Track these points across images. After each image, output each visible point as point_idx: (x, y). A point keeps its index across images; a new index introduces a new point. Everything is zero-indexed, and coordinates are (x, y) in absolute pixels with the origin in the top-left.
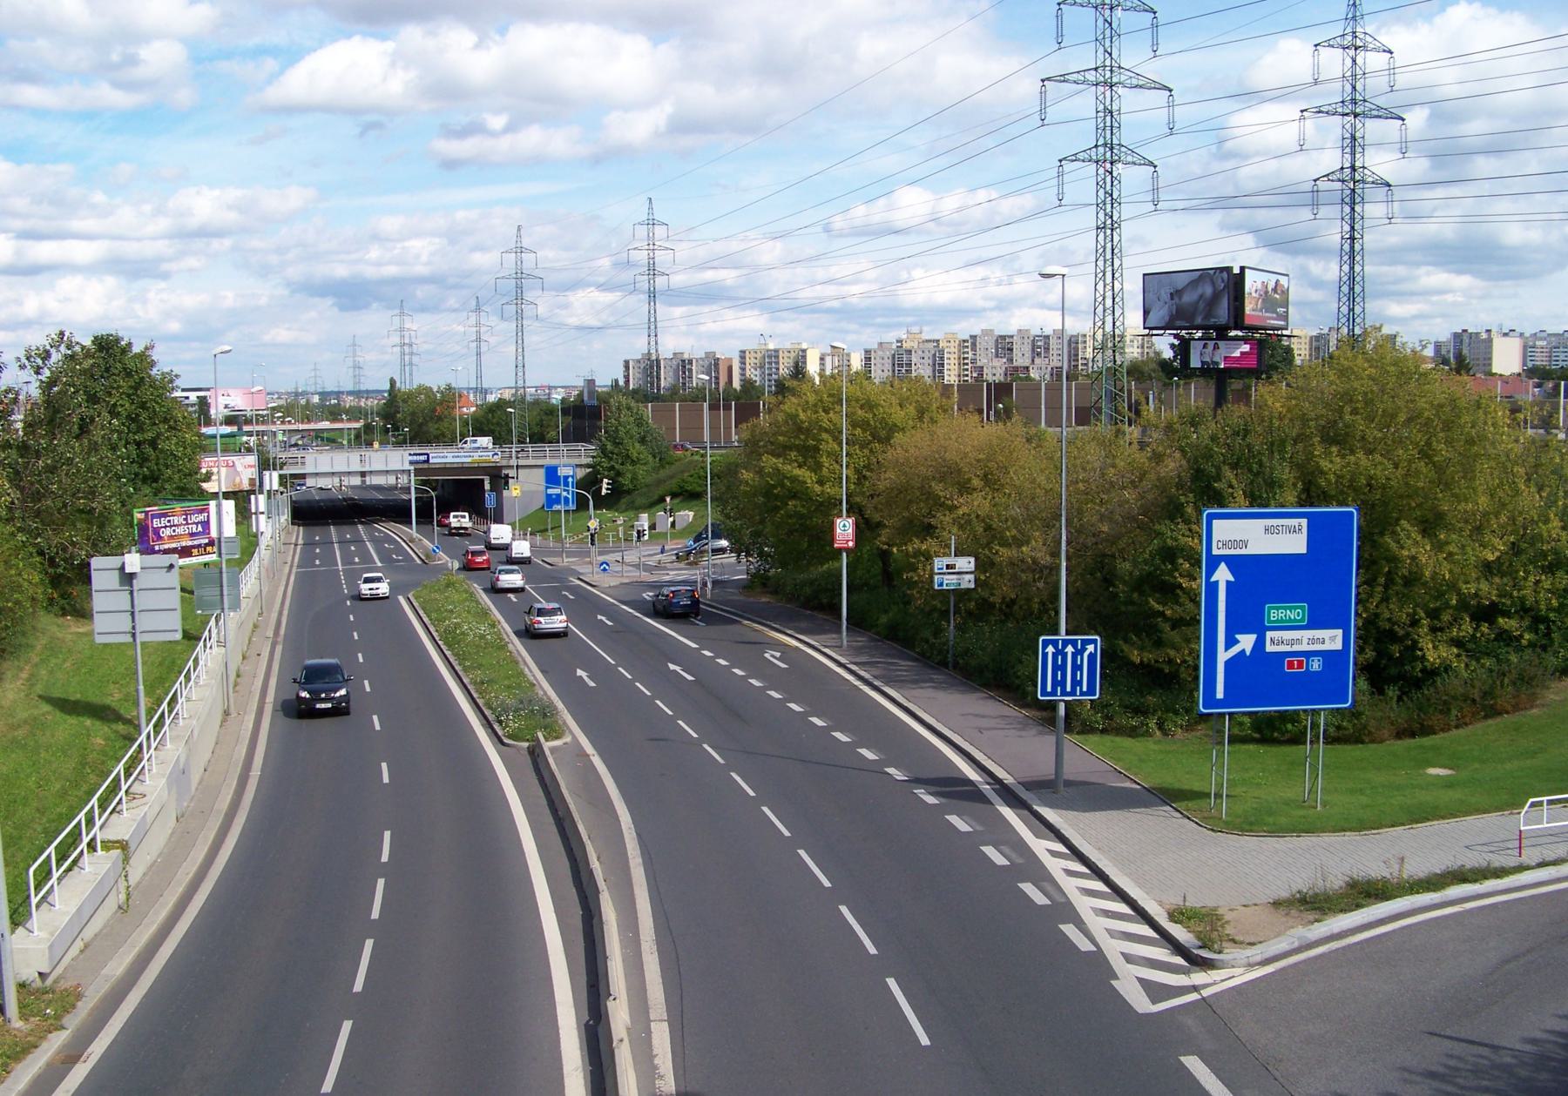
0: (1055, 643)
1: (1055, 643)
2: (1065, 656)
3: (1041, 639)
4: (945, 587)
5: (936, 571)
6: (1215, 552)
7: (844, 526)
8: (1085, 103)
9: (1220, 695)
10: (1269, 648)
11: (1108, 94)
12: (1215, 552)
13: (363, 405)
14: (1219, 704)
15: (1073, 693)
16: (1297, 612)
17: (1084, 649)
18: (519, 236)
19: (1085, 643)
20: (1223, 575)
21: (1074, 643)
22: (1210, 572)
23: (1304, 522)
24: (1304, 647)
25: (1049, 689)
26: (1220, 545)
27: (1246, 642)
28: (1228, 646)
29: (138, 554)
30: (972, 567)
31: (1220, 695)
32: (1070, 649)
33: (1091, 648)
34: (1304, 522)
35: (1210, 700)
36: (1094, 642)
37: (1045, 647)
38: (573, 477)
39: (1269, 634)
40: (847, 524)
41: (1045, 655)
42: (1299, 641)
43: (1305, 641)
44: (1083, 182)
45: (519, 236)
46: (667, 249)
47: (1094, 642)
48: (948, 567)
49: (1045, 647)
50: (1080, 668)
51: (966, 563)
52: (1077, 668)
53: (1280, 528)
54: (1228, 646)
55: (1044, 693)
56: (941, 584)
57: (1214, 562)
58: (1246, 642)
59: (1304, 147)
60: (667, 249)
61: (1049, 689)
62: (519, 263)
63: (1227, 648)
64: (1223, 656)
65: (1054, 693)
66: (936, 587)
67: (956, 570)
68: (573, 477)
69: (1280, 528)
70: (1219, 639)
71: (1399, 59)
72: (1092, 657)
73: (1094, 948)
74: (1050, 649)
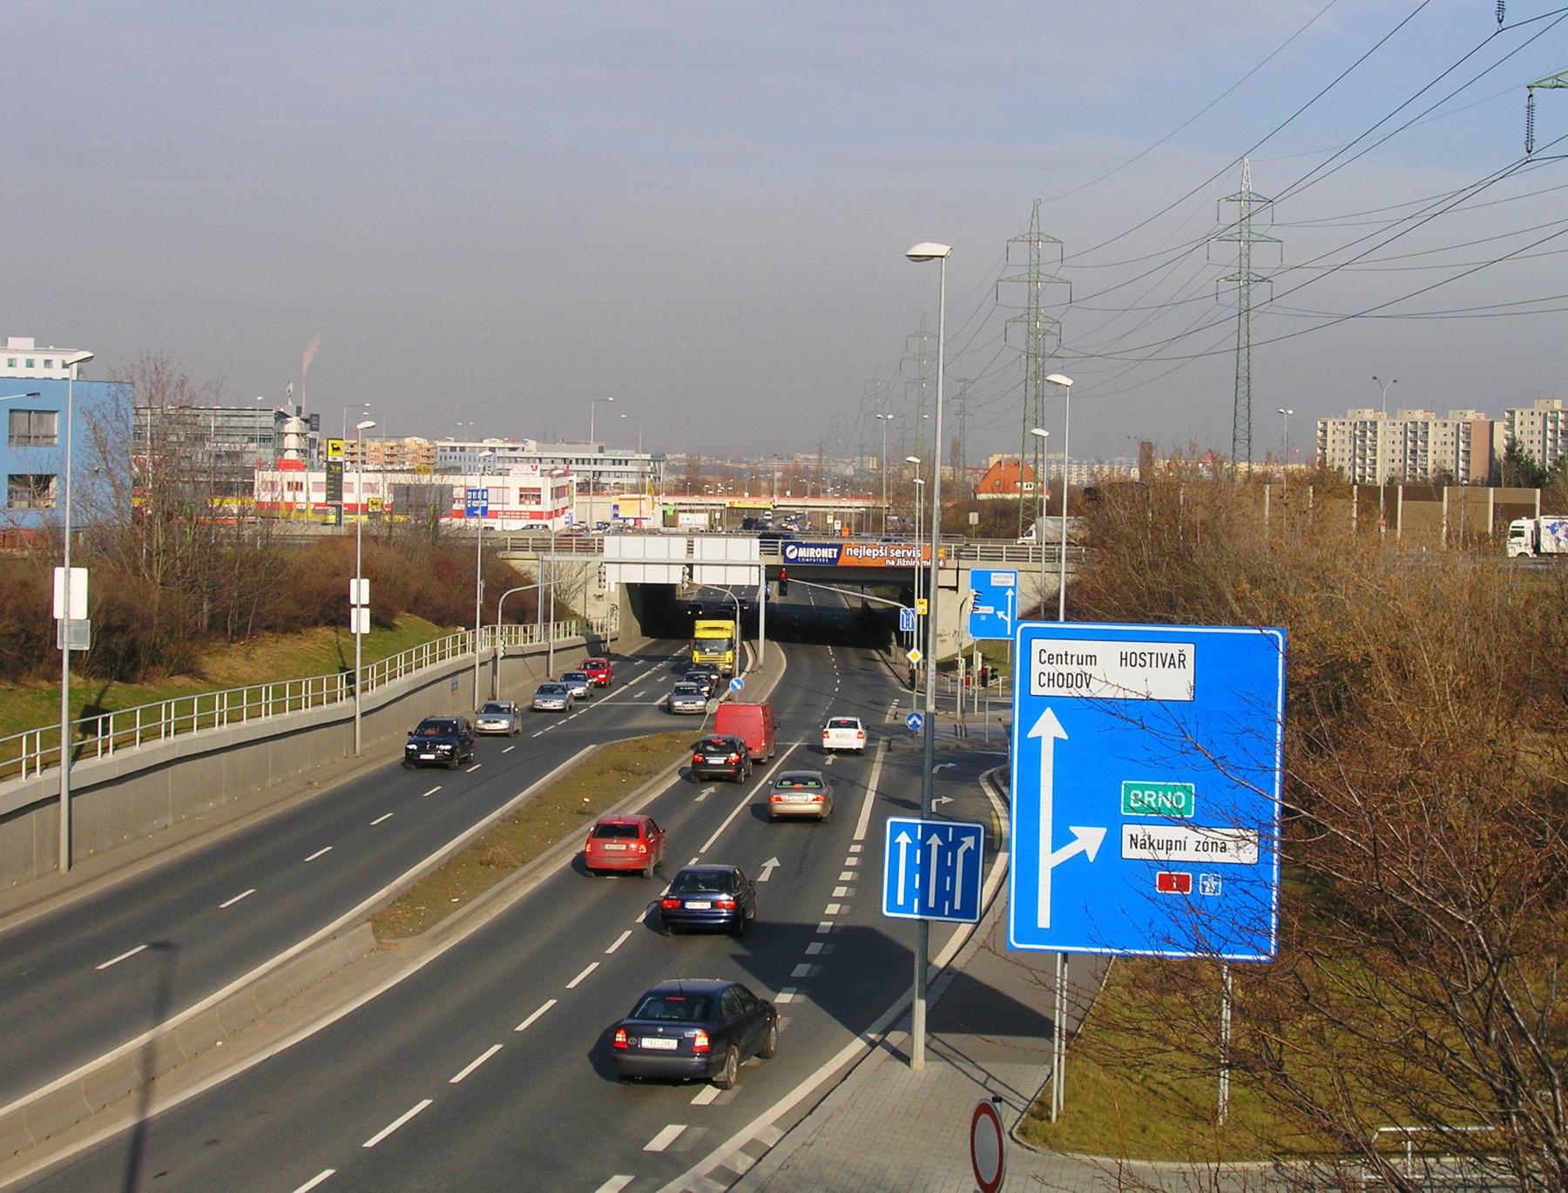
1: (911, 829)
6: (1036, 690)
9: (1044, 921)
10: (1129, 852)
12: (1036, 690)
14: (1042, 936)
15: (938, 910)
16: (1181, 797)
18: (1035, 214)
20: (1048, 728)
22: (1027, 724)
23: (1189, 649)
24: (1189, 855)
25: (900, 901)
26: (1044, 680)
27: (1089, 839)
28: (1057, 844)
31: (1044, 921)
32: (935, 841)
33: (969, 842)
34: (1189, 649)
35: (893, 906)
36: (976, 832)
37: (895, 835)
39: (1128, 830)
41: (895, 847)
42: (1180, 844)
43: (1191, 845)
45: (1035, 214)
46: (1270, 240)
47: (976, 832)
50: (952, 871)
52: (945, 871)
53: (1147, 658)
54: (1057, 844)
55: (893, 906)
57: (1034, 707)
58: (1089, 839)
59: (1504, 24)
60: (1270, 240)
61: (900, 901)
63: (1055, 847)
64: (1049, 859)
65: (907, 907)
68: (1014, 588)
69: (1147, 658)
74: (904, 839)
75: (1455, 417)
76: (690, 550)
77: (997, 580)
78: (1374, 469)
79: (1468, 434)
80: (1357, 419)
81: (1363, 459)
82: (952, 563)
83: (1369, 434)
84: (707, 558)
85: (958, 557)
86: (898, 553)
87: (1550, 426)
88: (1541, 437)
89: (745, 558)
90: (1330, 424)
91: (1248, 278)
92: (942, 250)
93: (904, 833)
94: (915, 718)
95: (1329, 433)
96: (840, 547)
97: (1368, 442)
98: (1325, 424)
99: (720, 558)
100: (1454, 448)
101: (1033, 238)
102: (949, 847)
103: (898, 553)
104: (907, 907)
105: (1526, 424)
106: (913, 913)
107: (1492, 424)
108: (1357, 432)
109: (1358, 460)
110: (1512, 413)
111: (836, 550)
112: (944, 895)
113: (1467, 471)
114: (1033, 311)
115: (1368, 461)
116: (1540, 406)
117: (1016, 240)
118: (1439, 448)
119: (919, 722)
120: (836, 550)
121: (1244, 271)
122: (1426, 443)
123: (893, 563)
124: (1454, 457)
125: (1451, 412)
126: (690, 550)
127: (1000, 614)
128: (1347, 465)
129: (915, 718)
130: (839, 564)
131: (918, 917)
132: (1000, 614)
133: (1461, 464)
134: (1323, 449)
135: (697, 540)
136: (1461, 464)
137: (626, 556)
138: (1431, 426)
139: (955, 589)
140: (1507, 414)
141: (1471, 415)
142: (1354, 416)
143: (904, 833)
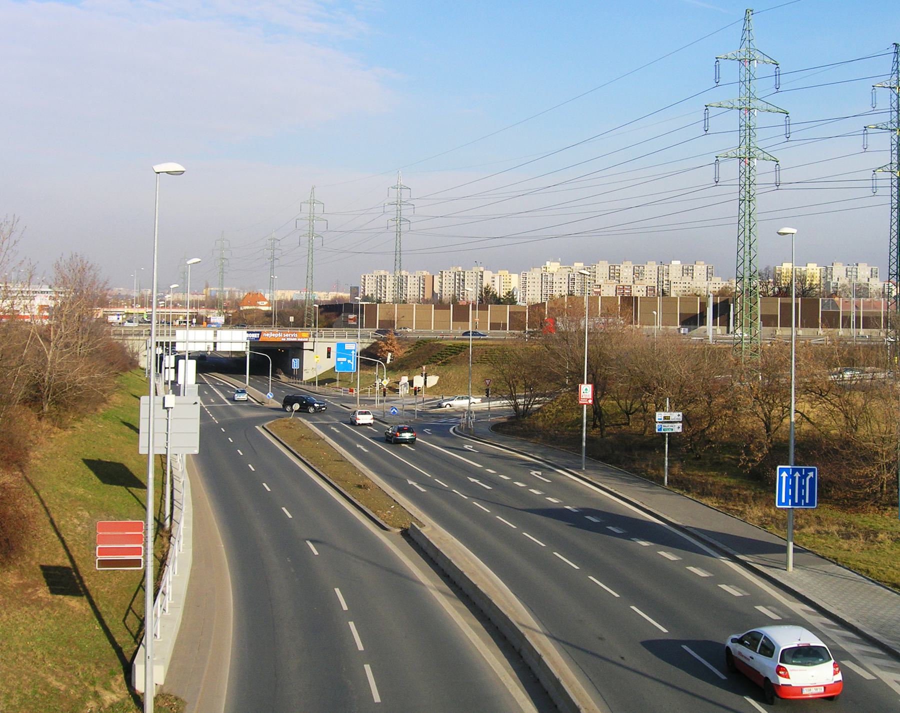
0: (787, 470)
1: (787, 470)
2: (794, 479)
3: (779, 467)
4: (663, 431)
5: (657, 420)
7: (586, 389)
8: (733, 119)
11: (747, 115)
13: (181, 298)
15: (799, 504)
17: (806, 475)
18: (313, 192)
19: (807, 471)
21: (800, 471)
25: (783, 501)
29: (174, 395)
30: (681, 418)
32: (797, 475)
33: (811, 474)
35: (780, 503)
36: (813, 470)
37: (780, 473)
38: (355, 350)
40: (588, 389)
41: (781, 478)
44: (731, 170)
45: (313, 192)
47: (813, 470)
48: (665, 418)
49: (780, 473)
51: (676, 416)
52: (802, 487)
56: (660, 429)
61: (783, 501)
62: (312, 210)
65: (786, 503)
66: (657, 431)
67: (671, 420)
68: (355, 350)
70: (269, 438)
71: (793, 118)
72: (812, 480)
73: (67, 563)
74: (784, 475)
75: (419, 274)
76: (215, 335)
77: (347, 347)
78: (385, 295)
79: (424, 280)
80: (378, 274)
81: (381, 291)
82: (312, 339)
83: (383, 280)
84: (223, 339)
85: (314, 337)
86: (287, 335)
87: (457, 277)
88: (453, 282)
89: (240, 339)
90: (367, 276)
91: (400, 219)
92: (795, 231)
93: (797, 473)
94: (394, 410)
95: (367, 280)
96: (260, 333)
97: (383, 284)
98: (365, 276)
99: (229, 339)
100: (418, 286)
101: (312, 202)
102: (801, 478)
103: (287, 335)
104: (786, 503)
105: (447, 276)
106: (788, 505)
107: (433, 276)
108: (378, 280)
109: (379, 291)
110: (442, 272)
111: (258, 334)
112: (802, 497)
113: (424, 296)
114: (311, 232)
115: (383, 292)
116: (453, 270)
117: (304, 202)
118: (412, 286)
119: (396, 411)
120: (258, 334)
121: (399, 216)
122: (407, 284)
123: (284, 340)
124: (418, 290)
125: (375, 271)
126: (215, 335)
127: (349, 361)
128: (374, 293)
129: (394, 410)
130: (260, 340)
131: (790, 507)
132: (349, 361)
133: (421, 293)
134: (364, 287)
135: (219, 332)
136: (421, 293)
137: (197, 339)
138: (409, 277)
139: (313, 350)
140: (440, 273)
141: (425, 273)
142: (377, 273)
143: (797, 473)
